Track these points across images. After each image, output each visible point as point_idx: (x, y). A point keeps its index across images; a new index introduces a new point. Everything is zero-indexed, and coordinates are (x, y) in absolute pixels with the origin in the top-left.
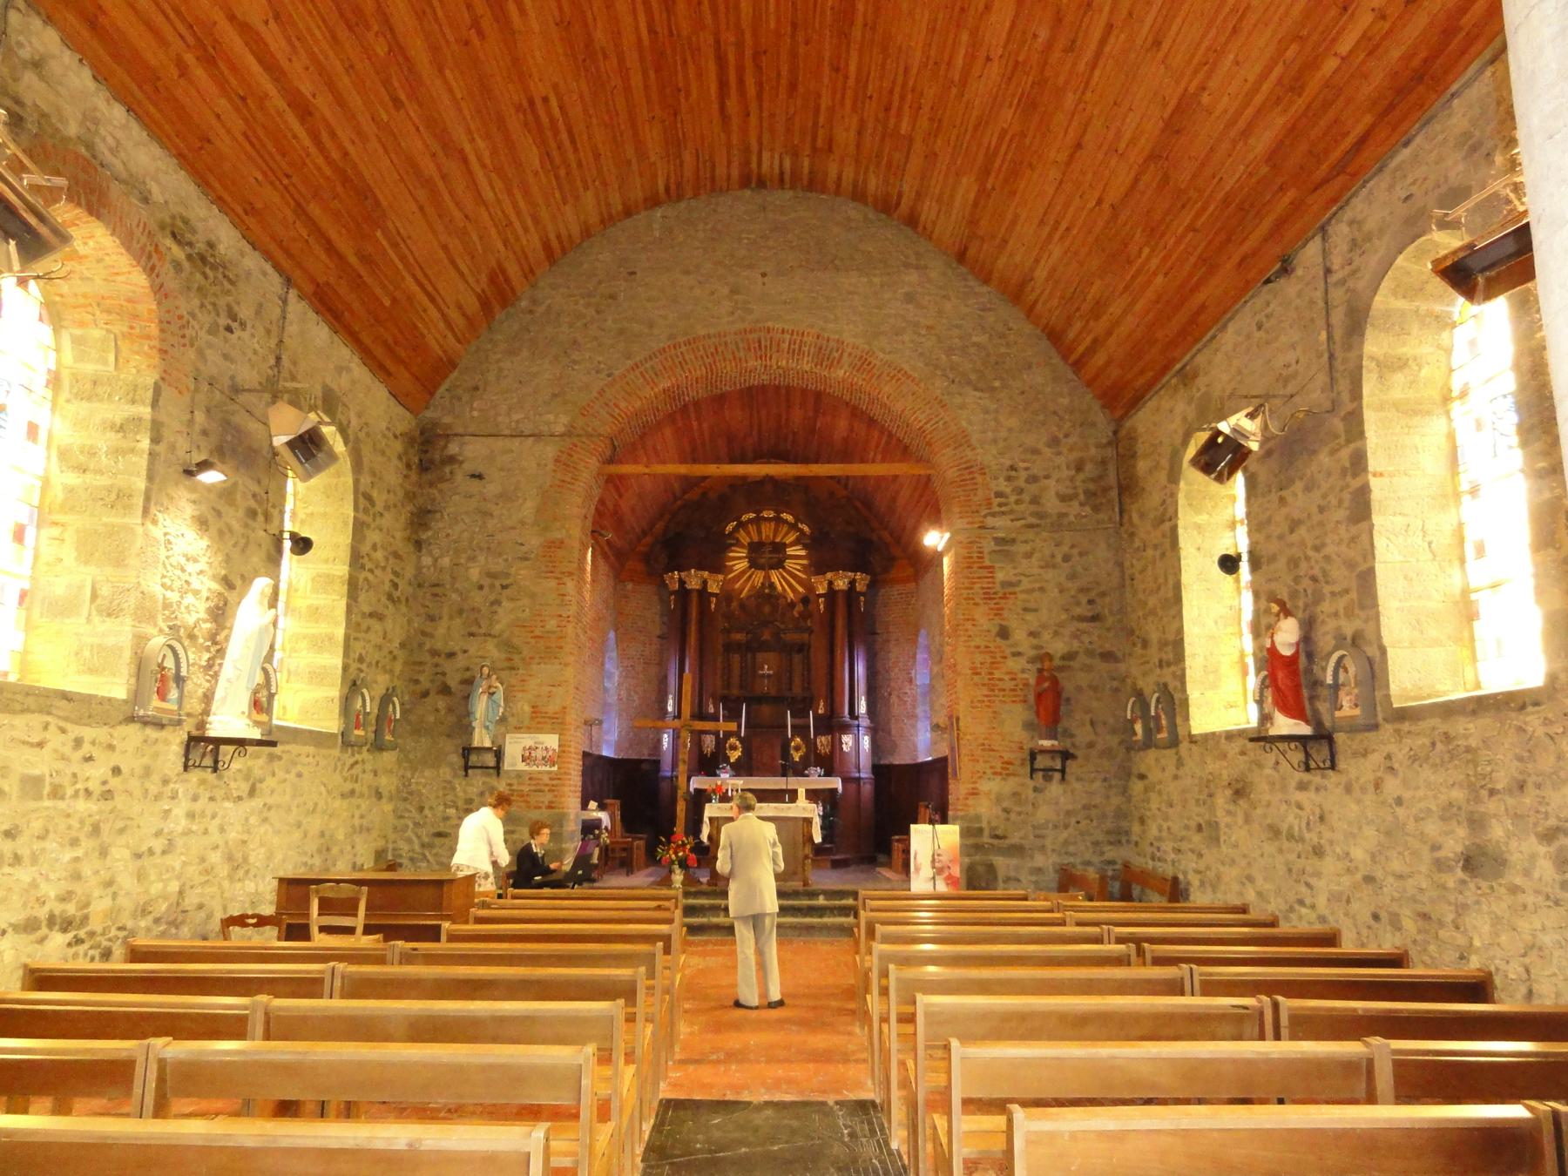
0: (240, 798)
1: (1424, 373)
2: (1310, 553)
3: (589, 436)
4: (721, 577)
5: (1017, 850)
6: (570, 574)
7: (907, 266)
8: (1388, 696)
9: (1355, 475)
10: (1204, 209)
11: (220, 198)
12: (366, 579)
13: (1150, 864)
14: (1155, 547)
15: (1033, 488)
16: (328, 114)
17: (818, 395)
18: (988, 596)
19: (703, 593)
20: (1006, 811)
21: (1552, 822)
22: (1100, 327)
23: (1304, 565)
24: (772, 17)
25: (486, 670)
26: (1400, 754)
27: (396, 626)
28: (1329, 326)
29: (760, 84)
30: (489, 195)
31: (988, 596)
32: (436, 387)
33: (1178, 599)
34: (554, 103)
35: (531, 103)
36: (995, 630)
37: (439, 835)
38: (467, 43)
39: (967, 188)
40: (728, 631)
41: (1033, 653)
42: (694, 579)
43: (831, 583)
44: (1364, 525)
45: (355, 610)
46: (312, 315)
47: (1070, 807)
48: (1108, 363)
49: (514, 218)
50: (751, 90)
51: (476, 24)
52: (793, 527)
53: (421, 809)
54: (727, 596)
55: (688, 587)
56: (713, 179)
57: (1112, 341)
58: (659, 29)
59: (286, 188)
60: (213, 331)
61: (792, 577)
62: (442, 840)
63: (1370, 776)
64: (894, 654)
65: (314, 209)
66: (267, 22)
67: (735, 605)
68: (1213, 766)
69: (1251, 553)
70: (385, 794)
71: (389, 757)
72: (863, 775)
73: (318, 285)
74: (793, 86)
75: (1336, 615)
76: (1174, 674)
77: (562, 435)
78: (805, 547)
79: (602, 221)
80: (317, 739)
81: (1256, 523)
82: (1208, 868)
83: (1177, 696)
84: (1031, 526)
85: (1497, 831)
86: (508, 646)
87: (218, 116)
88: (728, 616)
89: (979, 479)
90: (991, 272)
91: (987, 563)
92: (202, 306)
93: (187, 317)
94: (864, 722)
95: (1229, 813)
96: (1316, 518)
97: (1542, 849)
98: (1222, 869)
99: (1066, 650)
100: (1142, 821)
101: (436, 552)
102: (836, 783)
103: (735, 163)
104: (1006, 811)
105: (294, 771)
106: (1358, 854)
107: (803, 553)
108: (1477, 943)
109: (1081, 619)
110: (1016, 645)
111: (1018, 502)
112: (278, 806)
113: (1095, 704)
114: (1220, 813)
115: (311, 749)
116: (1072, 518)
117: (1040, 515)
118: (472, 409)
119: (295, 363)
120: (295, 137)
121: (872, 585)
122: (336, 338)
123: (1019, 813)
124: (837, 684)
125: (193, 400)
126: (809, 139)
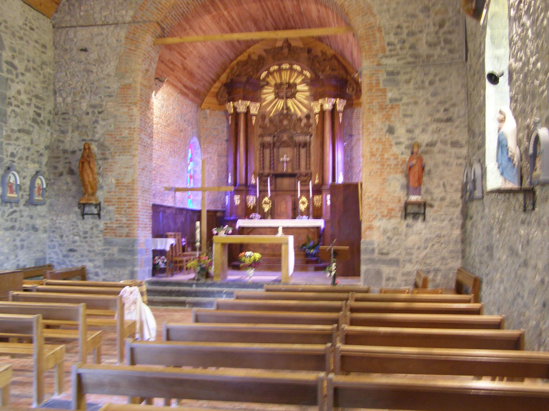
3: (145, 22)
4: (258, 104)
5: (395, 262)
6: (135, 104)
12: (13, 111)
15: (411, 40)
18: (382, 108)
20: (389, 238)
37: (71, 250)
41: (409, 142)
42: (241, 106)
43: (322, 106)
47: (428, 236)
52: (301, 73)
53: (62, 236)
54: (262, 116)
61: (302, 103)
67: (267, 120)
71: (42, 209)
77: (129, 23)
78: (308, 84)
88: (263, 127)
89: (378, 35)
99: (429, 140)
101: (64, 95)
110: (398, 137)
117: (416, 57)
118: (80, 10)
121: (345, 108)
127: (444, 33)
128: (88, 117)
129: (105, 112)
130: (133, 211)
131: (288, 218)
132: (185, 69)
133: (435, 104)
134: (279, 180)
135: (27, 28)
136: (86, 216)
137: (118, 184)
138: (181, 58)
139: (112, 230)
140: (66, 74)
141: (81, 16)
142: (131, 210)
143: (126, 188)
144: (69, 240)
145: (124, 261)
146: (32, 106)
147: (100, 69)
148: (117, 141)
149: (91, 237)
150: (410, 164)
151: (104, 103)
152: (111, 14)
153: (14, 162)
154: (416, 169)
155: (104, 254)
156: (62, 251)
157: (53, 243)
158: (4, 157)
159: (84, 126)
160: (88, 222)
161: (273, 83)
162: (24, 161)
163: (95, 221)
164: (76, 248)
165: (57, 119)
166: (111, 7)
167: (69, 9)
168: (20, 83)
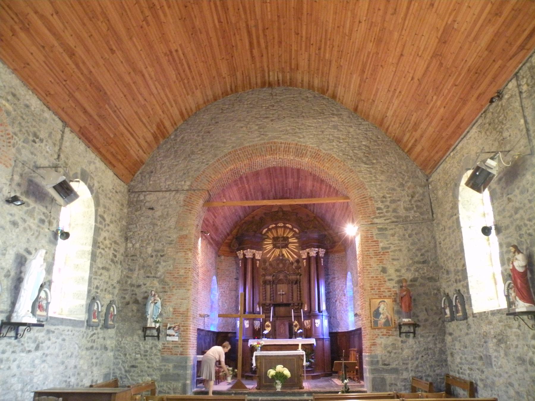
0: (29, 351)
2: (528, 222)
3: (199, 190)
4: (261, 252)
5: (395, 371)
7: (333, 114)
10: (460, 74)
11: (34, 89)
12: (100, 253)
13: (457, 376)
14: (449, 228)
15: (393, 206)
16: (83, 56)
17: (298, 170)
18: (377, 254)
19: (253, 259)
20: (390, 352)
22: (417, 135)
23: (524, 229)
24: (269, 13)
25: (153, 293)
27: (116, 274)
28: (524, 117)
29: (266, 42)
30: (155, 91)
31: (377, 254)
32: (135, 173)
33: (462, 250)
34: (180, 52)
35: (171, 52)
36: (380, 269)
37: (133, 366)
38: (142, 27)
39: (355, 79)
40: (264, 275)
42: (249, 254)
43: (308, 253)
45: (94, 266)
46: (76, 139)
48: (423, 150)
49: (166, 101)
50: (263, 45)
51: (145, 19)
52: (291, 230)
53: (125, 355)
55: (247, 257)
56: (250, 84)
57: (424, 139)
58: (222, 20)
59: (64, 85)
60: (26, 141)
62: (134, 369)
64: (338, 283)
65: (77, 95)
66: (52, 15)
67: (267, 264)
68: (485, 328)
70: (110, 348)
71: (111, 332)
72: (325, 337)
73: (81, 127)
74: (280, 42)
76: (463, 285)
77: (187, 190)
78: (297, 238)
79: (205, 103)
80: (74, 323)
81: (498, 212)
82: (487, 378)
83: (465, 296)
84: (393, 222)
86: (162, 281)
87: (32, 54)
88: (265, 269)
90: (369, 115)
92: (20, 131)
93: (11, 134)
94: (325, 314)
95: (496, 350)
96: (528, 205)
99: (412, 277)
100: (452, 354)
101: (134, 242)
102: (313, 341)
103: (259, 77)
104: (390, 352)
105: (61, 338)
107: (296, 241)
110: (389, 275)
111: (387, 212)
112: (51, 354)
113: (427, 301)
114: (491, 351)
115: (70, 328)
116: (411, 218)
119: (67, 159)
120: (68, 64)
121: (326, 254)
122: (88, 149)
123: (395, 353)
124: (312, 299)
125: (13, 171)
126: (288, 64)
127: (415, 202)
128: (152, 259)
129: (166, 255)
130: (187, 334)
131: (285, 338)
132: (214, 225)
133: (414, 251)
134: (277, 308)
135: (114, 191)
136: (146, 338)
137: (175, 311)
138: (213, 217)
139: (169, 349)
140: (136, 226)
141: (150, 184)
142: (185, 333)
143: (181, 315)
144: (131, 358)
145: (179, 375)
146: (112, 249)
147: (163, 223)
148: (175, 278)
149: (150, 355)
150: (402, 295)
151: (165, 249)
152: (173, 183)
153: (97, 293)
154: (406, 299)
155: (161, 370)
156: (124, 367)
157: (117, 360)
158: (92, 289)
159: (149, 266)
160: (148, 343)
161: (271, 236)
162: (104, 292)
163: (154, 342)
164: (137, 365)
165: (127, 260)
166: (173, 178)
167: (142, 178)
168: (107, 232)
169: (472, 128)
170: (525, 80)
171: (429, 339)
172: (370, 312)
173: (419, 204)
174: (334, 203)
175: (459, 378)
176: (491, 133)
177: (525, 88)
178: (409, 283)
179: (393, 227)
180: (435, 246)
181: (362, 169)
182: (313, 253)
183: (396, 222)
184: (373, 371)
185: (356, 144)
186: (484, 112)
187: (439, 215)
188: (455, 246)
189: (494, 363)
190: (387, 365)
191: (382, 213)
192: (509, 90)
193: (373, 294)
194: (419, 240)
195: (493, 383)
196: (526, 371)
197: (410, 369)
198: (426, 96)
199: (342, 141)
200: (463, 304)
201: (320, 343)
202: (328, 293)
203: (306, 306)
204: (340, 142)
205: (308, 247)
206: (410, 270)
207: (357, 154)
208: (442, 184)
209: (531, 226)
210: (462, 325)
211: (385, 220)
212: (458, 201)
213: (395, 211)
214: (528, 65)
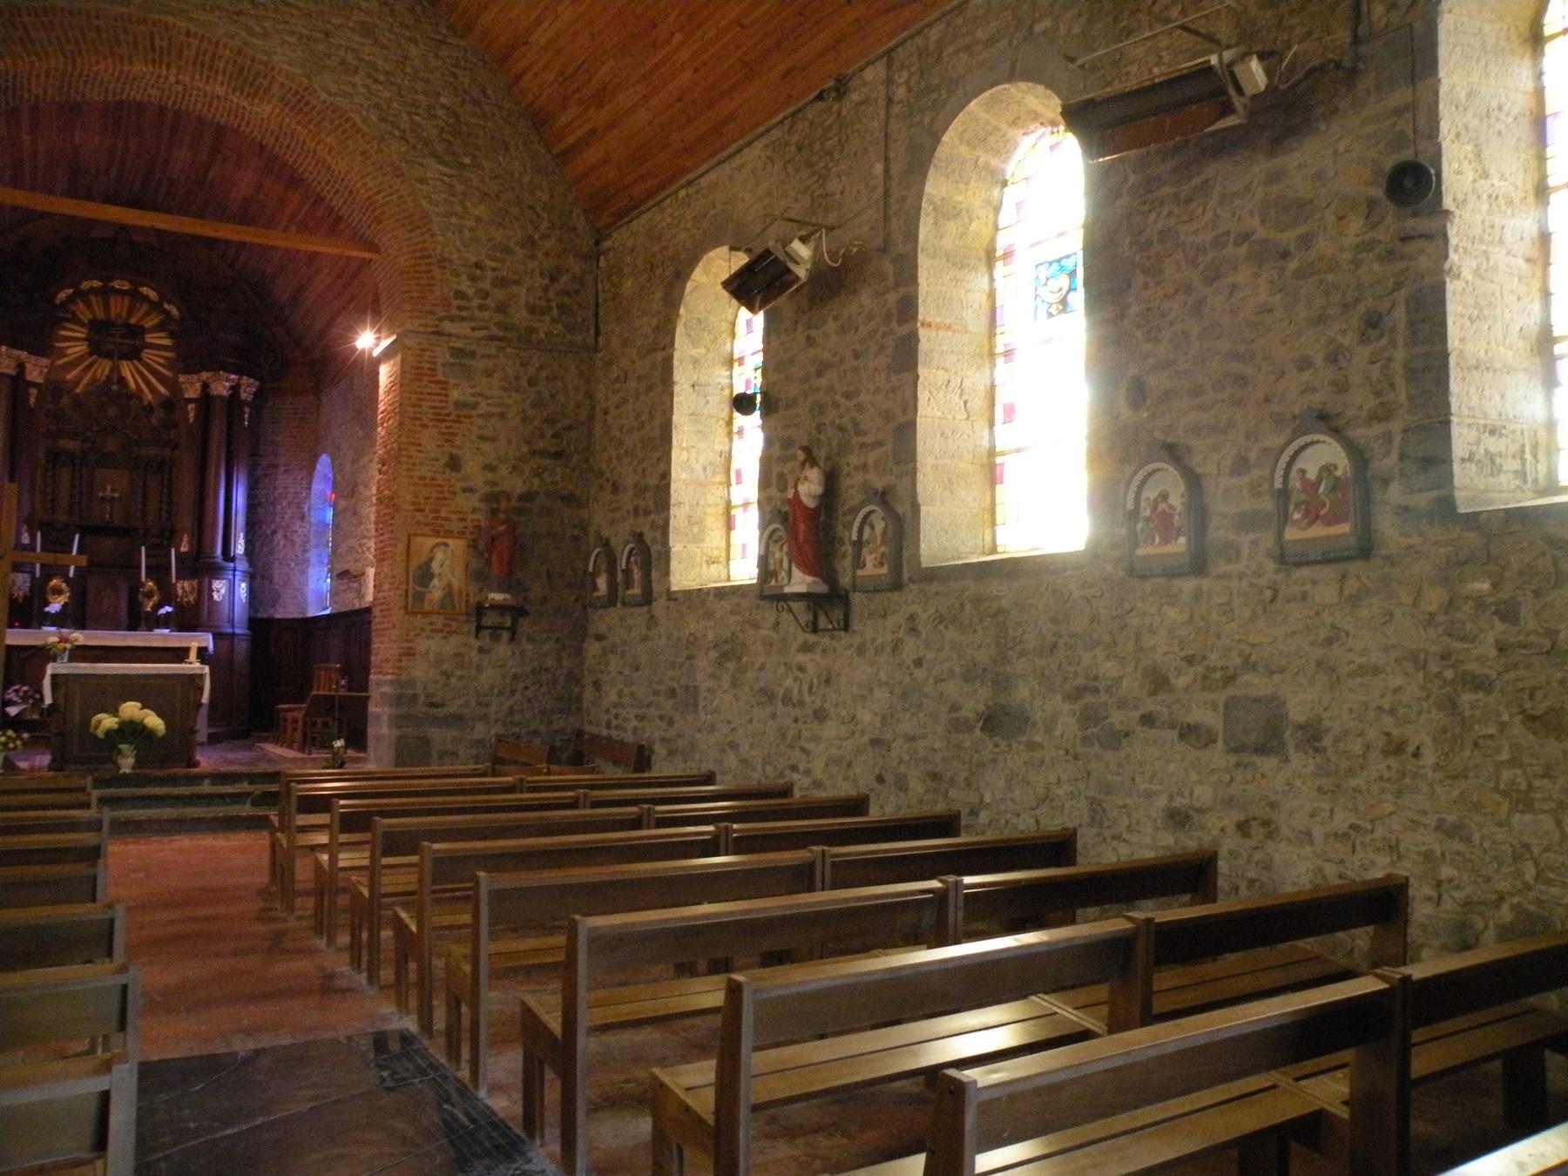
1: (974, 226)
4: (45, 361)
5: (457, 720)
8: (917, 555)
9: (901, 321)
13: (605, 732)
14: (639, 379)
15: (500, 294)
18: (439, 418)
20: (445, 674)
21: (1080, 681)
23: (831, 414)
26: (925, 616)
28: (887, 159)
31: (439, 418)
36: (444, 460)
41: (488, 489)
43: (205, 386)
44: (905, 375)
48: (605, 161)
52: (156, 306)
54: (54, 388)
63: (889, 637)
64: (284, 481)
67: (66, 400)
68: (695, 625)
69: (764, 394)
72: (237, 631)
75: (865, 466)
78: (172, 335)
84: (492, 338)
85: (1023, 692)
89: (437, 273)
91: (440, 377)
94: (242, 565)
95: (712, 676)
97: (1067, 707)
98: (698, 736)
99: (525, 489)
100: (597, 685)
104: (445, 674)
106: (865, 717)
107: (168, 342)
108: (987, 799)
109: (544, 454)
111: (481, 308)
114: (700, 677)
121: (259, 394)
123: (461, 678)
131: (115, 626)
161: (86, 317)
169: (750, 144)
170: (905, 74)
171: (546, 647)
172: (407, 567)
173: (566, 300)
174: (316, 254)
175: (609, 739)
176: (798, 170)
177: (901, 92)
178: (514, 503)
179: (493, 351)
180: (591, 419)
181: (429, 174)
182: (221, 388)
183: (501, 339)
184: (398, 721)
185: (421, 97)
186: (794, 114)
187: (615, 342)
188: (647, 427)
189: (701, 704)
190: (438, 706)
191: (467, 309)
192: (865, 84)
193: (418, 523)
194: (553, 396)
195: (693, 745)
196: (774, 716)
197: (493, 717)
198: (655, 27)
199: (381, 78)
200: (647, 567)
201: (225, 644)
202: (252, 507)
203: (186, 538)
204: (376, 81)
205: (205, 368)
206: (522, 472)
207: (419, 126)
208: (639, 262)
209: (848, 410)
210: (638, 616)
211: (473, 329)
212: (678, 315)
213: (501, 308)
214: (919, 40)
